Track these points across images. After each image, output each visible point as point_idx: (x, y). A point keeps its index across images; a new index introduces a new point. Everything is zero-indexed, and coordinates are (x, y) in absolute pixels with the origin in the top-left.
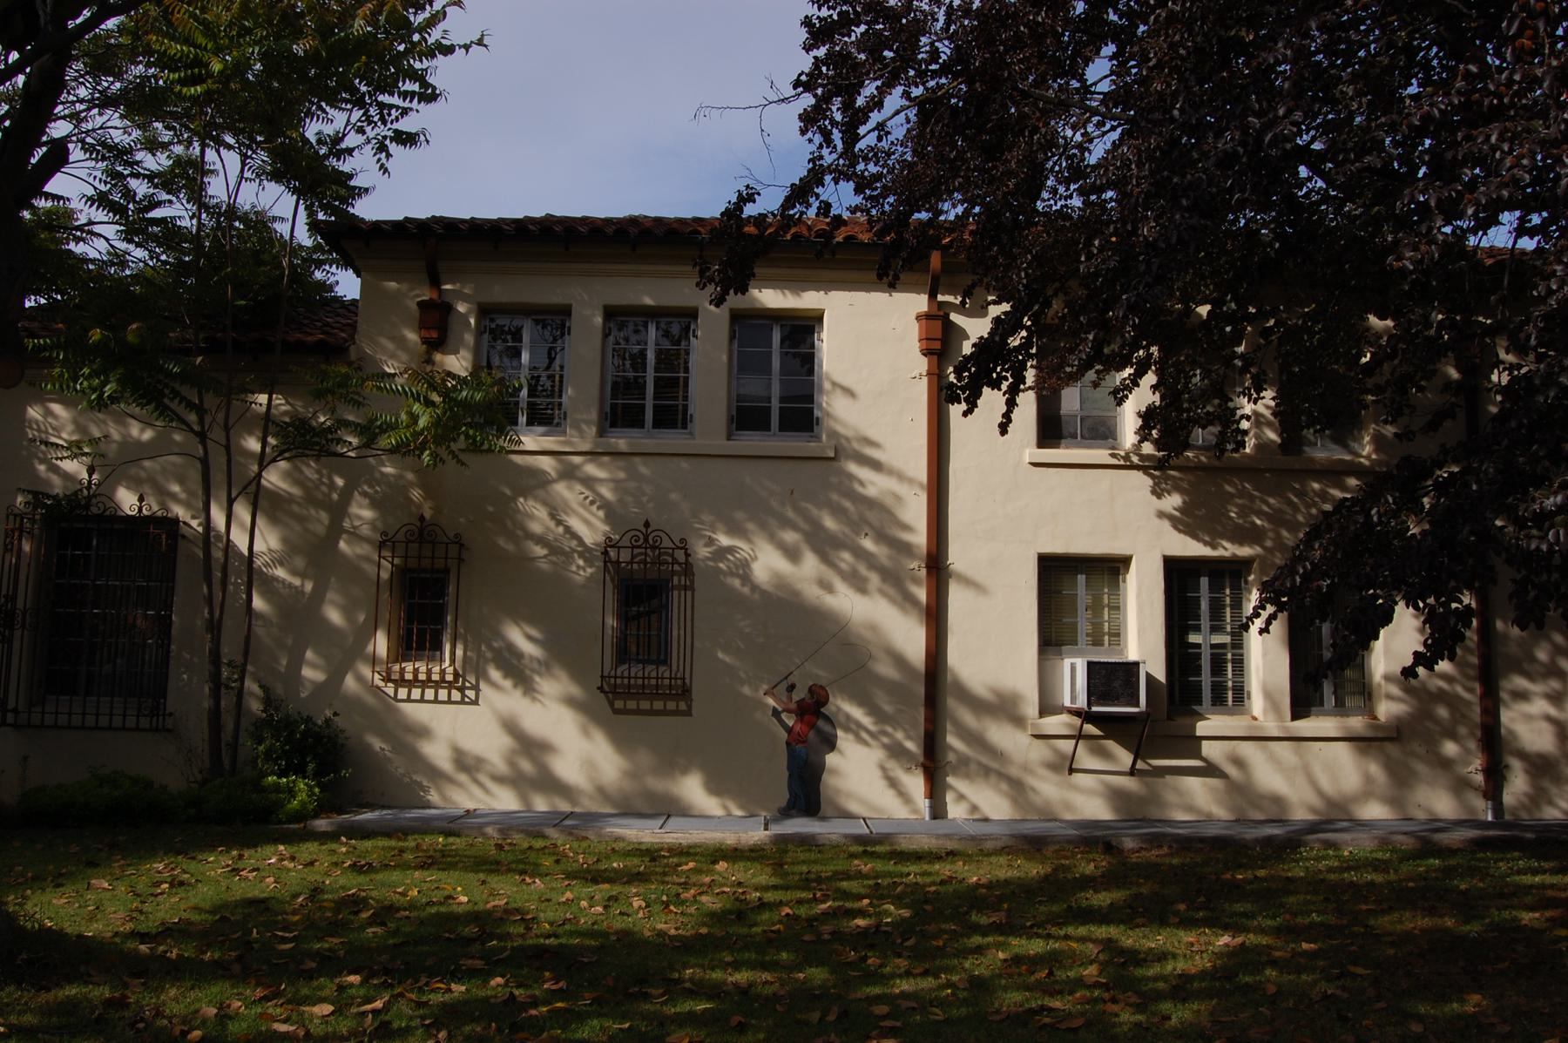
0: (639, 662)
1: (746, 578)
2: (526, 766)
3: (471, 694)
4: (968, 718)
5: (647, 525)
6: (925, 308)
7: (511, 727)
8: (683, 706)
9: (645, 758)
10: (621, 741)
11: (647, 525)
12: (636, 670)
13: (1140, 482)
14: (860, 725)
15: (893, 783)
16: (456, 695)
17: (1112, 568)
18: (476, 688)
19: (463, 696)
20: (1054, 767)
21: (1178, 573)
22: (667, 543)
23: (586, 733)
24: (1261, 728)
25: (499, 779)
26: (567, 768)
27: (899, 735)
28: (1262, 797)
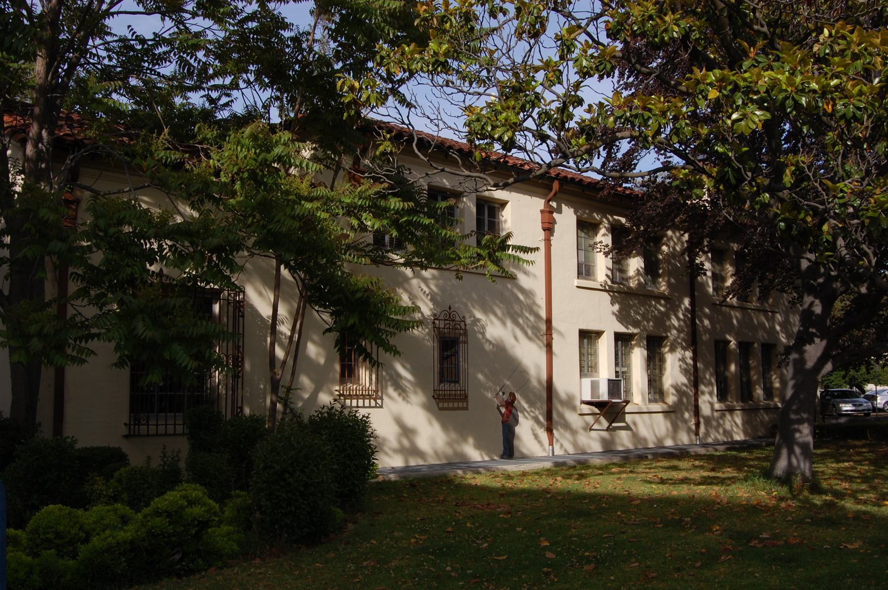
0: (448, 382)
1: (483, 334)
2: (406, 442)
3: (379, 401)
4: (560, 408)
5: (450, 308)
6: (542, 208)
7: (399, 422)
8: (465, 405)
9: (454, 435)
10: (445, 427)
11: (450, 308)
12: (447, 386)
13: (606, 297)
14: (525, 409)
15: (536, 436)
16: (373, 403)
17: (599, 334)
18: (382, 399)
19: (376, 403)
20: (585, 429)
21: (618, 337)
22: (458, 319)
23: (430, 423)
24: (640, 408)
25: (396, 451)
26: (423, 443)
27: (537, 412)
28: (641, 438)
